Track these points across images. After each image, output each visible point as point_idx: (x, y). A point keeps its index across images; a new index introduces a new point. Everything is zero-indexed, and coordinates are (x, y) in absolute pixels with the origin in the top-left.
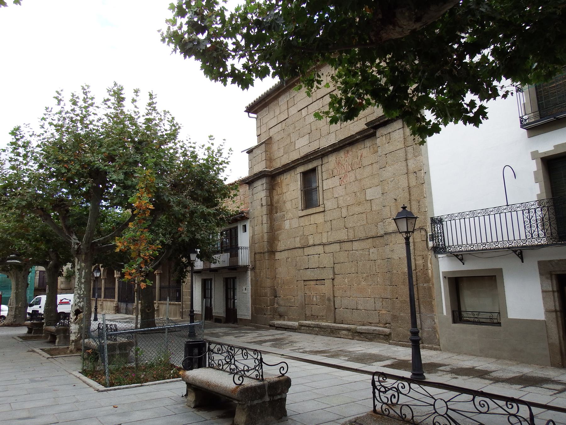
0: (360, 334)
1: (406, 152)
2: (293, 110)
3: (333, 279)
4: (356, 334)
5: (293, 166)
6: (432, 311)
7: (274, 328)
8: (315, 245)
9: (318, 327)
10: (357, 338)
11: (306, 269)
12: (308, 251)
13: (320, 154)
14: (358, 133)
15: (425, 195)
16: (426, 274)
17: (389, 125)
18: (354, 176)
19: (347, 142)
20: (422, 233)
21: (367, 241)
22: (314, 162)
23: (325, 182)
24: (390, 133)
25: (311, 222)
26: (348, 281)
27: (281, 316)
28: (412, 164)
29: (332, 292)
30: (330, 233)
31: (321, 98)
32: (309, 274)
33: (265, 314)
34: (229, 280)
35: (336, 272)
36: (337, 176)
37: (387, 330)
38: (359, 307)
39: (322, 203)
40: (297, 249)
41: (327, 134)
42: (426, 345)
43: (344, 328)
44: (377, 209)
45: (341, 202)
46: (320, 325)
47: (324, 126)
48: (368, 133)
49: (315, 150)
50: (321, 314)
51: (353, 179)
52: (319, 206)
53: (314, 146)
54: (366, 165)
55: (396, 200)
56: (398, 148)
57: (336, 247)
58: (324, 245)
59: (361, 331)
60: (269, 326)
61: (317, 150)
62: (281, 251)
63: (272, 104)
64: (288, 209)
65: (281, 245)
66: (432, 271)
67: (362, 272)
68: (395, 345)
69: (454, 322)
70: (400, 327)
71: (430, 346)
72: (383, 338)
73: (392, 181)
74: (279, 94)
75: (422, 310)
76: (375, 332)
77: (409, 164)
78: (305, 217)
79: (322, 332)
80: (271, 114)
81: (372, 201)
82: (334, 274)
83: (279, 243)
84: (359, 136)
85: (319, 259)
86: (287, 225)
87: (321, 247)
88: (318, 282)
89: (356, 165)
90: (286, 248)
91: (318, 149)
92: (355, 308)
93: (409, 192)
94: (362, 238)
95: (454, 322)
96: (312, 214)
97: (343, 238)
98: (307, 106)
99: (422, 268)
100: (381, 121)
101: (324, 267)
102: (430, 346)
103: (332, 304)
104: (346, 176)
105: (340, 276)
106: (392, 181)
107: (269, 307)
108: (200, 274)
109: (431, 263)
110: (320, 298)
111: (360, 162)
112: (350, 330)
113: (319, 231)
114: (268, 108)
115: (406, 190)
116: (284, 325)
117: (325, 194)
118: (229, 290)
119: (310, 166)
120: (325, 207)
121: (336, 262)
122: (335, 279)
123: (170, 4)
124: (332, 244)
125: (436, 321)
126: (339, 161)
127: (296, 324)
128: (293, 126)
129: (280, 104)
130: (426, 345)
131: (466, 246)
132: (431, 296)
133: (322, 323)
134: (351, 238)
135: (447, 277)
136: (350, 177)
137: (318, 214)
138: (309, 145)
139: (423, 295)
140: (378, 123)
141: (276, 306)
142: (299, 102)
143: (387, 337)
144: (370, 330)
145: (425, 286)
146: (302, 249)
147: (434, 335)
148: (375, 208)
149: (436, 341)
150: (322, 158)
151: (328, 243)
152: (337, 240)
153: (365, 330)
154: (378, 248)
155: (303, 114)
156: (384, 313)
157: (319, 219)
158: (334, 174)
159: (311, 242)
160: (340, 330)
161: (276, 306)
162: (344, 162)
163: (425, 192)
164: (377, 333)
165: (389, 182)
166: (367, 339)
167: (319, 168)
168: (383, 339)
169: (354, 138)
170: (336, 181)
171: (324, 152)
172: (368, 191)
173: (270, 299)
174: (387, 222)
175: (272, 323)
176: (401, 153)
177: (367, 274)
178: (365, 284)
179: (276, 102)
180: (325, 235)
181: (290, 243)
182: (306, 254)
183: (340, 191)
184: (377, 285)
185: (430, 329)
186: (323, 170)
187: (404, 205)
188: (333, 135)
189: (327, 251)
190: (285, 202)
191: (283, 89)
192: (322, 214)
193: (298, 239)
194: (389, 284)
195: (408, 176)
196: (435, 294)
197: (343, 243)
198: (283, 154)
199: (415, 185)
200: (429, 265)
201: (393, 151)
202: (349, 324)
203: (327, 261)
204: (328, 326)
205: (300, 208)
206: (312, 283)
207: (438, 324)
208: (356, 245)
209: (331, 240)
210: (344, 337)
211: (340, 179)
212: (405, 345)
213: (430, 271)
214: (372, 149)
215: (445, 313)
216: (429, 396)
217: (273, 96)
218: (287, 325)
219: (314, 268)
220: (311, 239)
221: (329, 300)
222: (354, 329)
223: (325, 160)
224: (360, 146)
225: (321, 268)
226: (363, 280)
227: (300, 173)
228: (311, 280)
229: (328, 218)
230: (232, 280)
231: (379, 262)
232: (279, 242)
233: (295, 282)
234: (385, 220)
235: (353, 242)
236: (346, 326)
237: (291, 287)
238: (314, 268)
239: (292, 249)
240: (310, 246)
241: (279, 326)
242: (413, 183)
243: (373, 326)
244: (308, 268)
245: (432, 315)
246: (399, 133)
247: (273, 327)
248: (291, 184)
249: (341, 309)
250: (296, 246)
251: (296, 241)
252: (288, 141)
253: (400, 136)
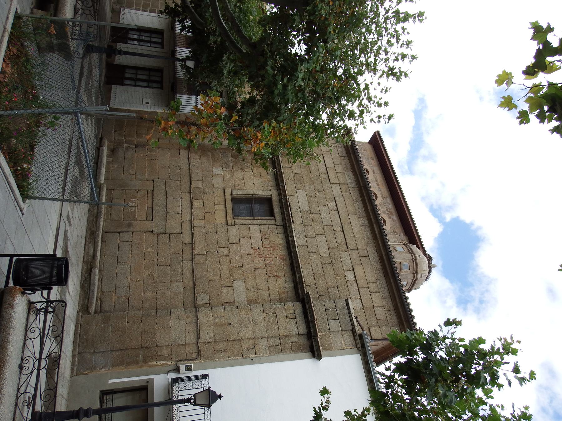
0: (89, 272)
1: (275, 337)
2: (336, 191)
3: (152, 232)
4: (89, 266)
5: (279, 187)
6: (114, 365)
7: (98, 146)
8: (192, 208)
9: (98, 213)
10: (85, 268)
11: (166, 193)
12: (186, 196)
13: (287, 226)
14: (301, 276)
15: (231, 358)
16: (152, 359)
17: (303, 318)
18: (260, 265)
19: (294, 263)
20: (194, 354)
21: (191, 279)
22: (280, 215)
23: (257, 227)
24: (296, 319)
25: (217, 206)
26: (149, 252)
27: (113, 151)
28: (263, 343)
29: (138, 230)
30: (203, 230)
31: (343, 229)
32: (160, 199)
33: (115, 131)
34: (160, 36)
35: (160, 236)
36: (262, 244)
37: (93, 310)
38: (120, 266)
39: (236, 223)
40: (189, 183)
41: (306, 234)
42: (76, 359)
43: (97, 251)
44: (223, 294)
45: (235, 248)
46: (100, 216)
47: (315, 231)
48: (300, 289)
49: (292, 217)
50: (113, 212)
51: (257, 265)
52: (234, 219)
53: (296, 216)
54: (269, 282)
55: (230, 324)
56: (280, 328)
57: (188, 240)
58: (191, 221)
59: (92, 274)
60: (100, 136)
61: (291, 219)
62: (188, 159)
63: (348, 162)
64: (235, 174)
65: (195, 159)
66: (155, 366)
67: (159, 272)
68: (77, 319)
69: (101, 391)
70: (96, 326)
71: (76, 363)
72: (85, 303)
73: (249, 320)
74: (356, 174)
75: (114, 353)
76: (91, 293)
77: (263, 340)
78: (223, 198)
79: (92, 218)
80: (337, 160)
81: (232, 287)
82: (158, 234)
83: (198, 157)
84: (298, 278)
85: (176, 214)
86: (218, 171)
87: (188, 217)
88: (150, 210)
89: (270, 270)
90: (192, 167)
91: (293, 221)
92: (119, 261)
93: (236, 340)
94: (194, 273)
95: (101, 391)
96: (226, 208)
97: (197, 248)
98: (337, 210)
99: (159, 354)
100: (308, 311)
101: (166, 221)
102: (76, 363)
103: (124, 230)
104: (261, 256)
105: (155, 241)
106: (249, 320)
107: (123, 138)
108: (170, 28)
109: (163, 364)
110: (132, 212)
111: (272, 274)
112: (94, 259)
113: (207, 215)
114: (344, 155)
115: (239, 337)
116: (101, 162)
117: (245, 227)
118: (148, 35)
119: (276, 210)
120: (231, 225)
121: (171, 237)
122: (152, 235)
123: (485, 340)
124: (191, 234)
125: (103, 370)
126: (277, 248)
127: (102, 180)
128: (321, 189)
129: (346, 173)
130: (76, 359)
131: (177, 416)
132: (129, 364)
133: (103, 218)
134: (197, 259)
135: (147, 384)
136: (259, 261)
137: (225, 215)
138: (299, 209)
139: (130, 355)
140: (307, 308)
141: (125, 145)
142: (343, 200)
143: (86, 309)
144: (94, 287)
145: (140, 357)
146: (188, 190)
147: (88, 367)
148: (224, 291)
149: (81, 370)
150: (283, 225)
151: (193, 227)
152: (195, 239)
153: (94, 281)
154: (182, 294)
155: (331, 204)
156: (112, 299)
157: (220, 218)
158: (264, 241)
159: (196, 203)
160: (95, 245)
161: (125, 145)
162: (275, 254)
163: (234, 358)
164: (90, 297)
165: (248, 316)
166: (84, 281)
167: (273, 222)
168: (84, 303)
169: (297, 271)
170: (257, 243)
171: (289, 231)
172: (242, 283)
173: (134, 141)
174: (209, 312)
175: (104, 142)
176: (274, 332)
177: (156, 278)
178: (146, 275)
179: (349, 167)
180: (202, 223)
181: (197, 173)
182: (183, 195)
183: (246, 247)
184: (144, 291)
185: (94, 363)
186: (270, 226)
187: (223, 396)
188: (304, 243)
189: (184, 225)
190: (242, 169)
191: (360, 181)
192: (224, 222)
193: (200, 185)
194: (143, 313)
195: (252, 339)
196: (131, 369)
197: (190, 248)
198: (294, 171)
199: (243, 346)
200: (161, 363)
201: (278, 322)
202: (101, 251)
203: (173, 225)
204: (99, 228)
205: (234, 192)
206: (150, 201)
207: (99, 373)
208: (187, 264)
209: (196, 231)
210: (86, 250)
211: (259, 248)
212: (76, 333)
213: (155, 363)
214: (283, 290)
215: (111, 381)
216: (20, 385)
217: (355, 166)
218: (101, 166)
219: (166, 206)
220: (199, 204)
221: (130, 225)
222: (95, 264)
223: (280, 230)
224: (289, 276)
225: (166, 216)
226: (149, 273)
227: (271, 195)
228: (153, 201)
229: (220, 229)
230: (160, 41)
231: (168, 294)
232: (199, 156)
233: (152, 177)
234: (210, 309)
235: (191, 262)
236: (98, 253)
237: (146, 170)
238: (166, 206)
239: (190, 174)
240: (191, 201)
241: (100, 154)
242: (245, 344)
243: (98, 283)
244: (167, 197)
245: (109, 365)
246: (295, 329)
247: (99, 143)
248: (260, 181)
249: (119, 241)
250: (193, 182)
251: (198, 182)
252: (307, 181)
253: (291, 330)
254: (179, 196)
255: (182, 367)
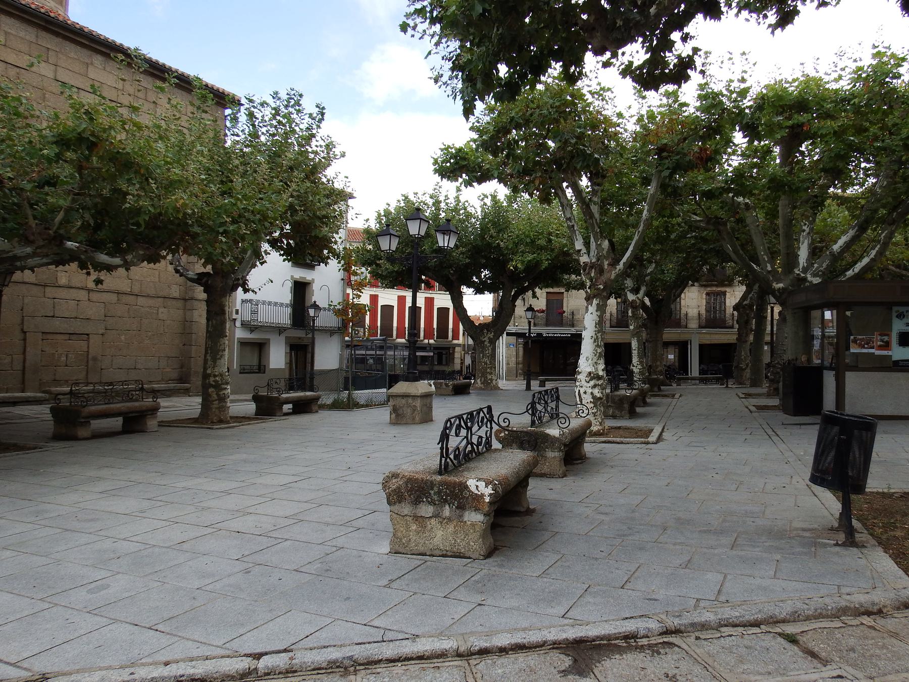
38: (139, 366)
57: (114, 297)
88: (73, 337)
254: (51, 301)
255: (235, 316)
